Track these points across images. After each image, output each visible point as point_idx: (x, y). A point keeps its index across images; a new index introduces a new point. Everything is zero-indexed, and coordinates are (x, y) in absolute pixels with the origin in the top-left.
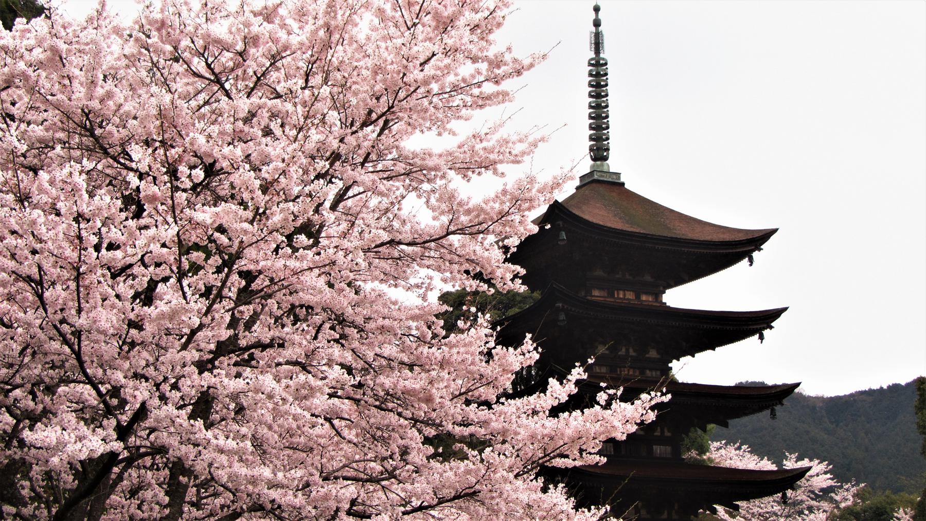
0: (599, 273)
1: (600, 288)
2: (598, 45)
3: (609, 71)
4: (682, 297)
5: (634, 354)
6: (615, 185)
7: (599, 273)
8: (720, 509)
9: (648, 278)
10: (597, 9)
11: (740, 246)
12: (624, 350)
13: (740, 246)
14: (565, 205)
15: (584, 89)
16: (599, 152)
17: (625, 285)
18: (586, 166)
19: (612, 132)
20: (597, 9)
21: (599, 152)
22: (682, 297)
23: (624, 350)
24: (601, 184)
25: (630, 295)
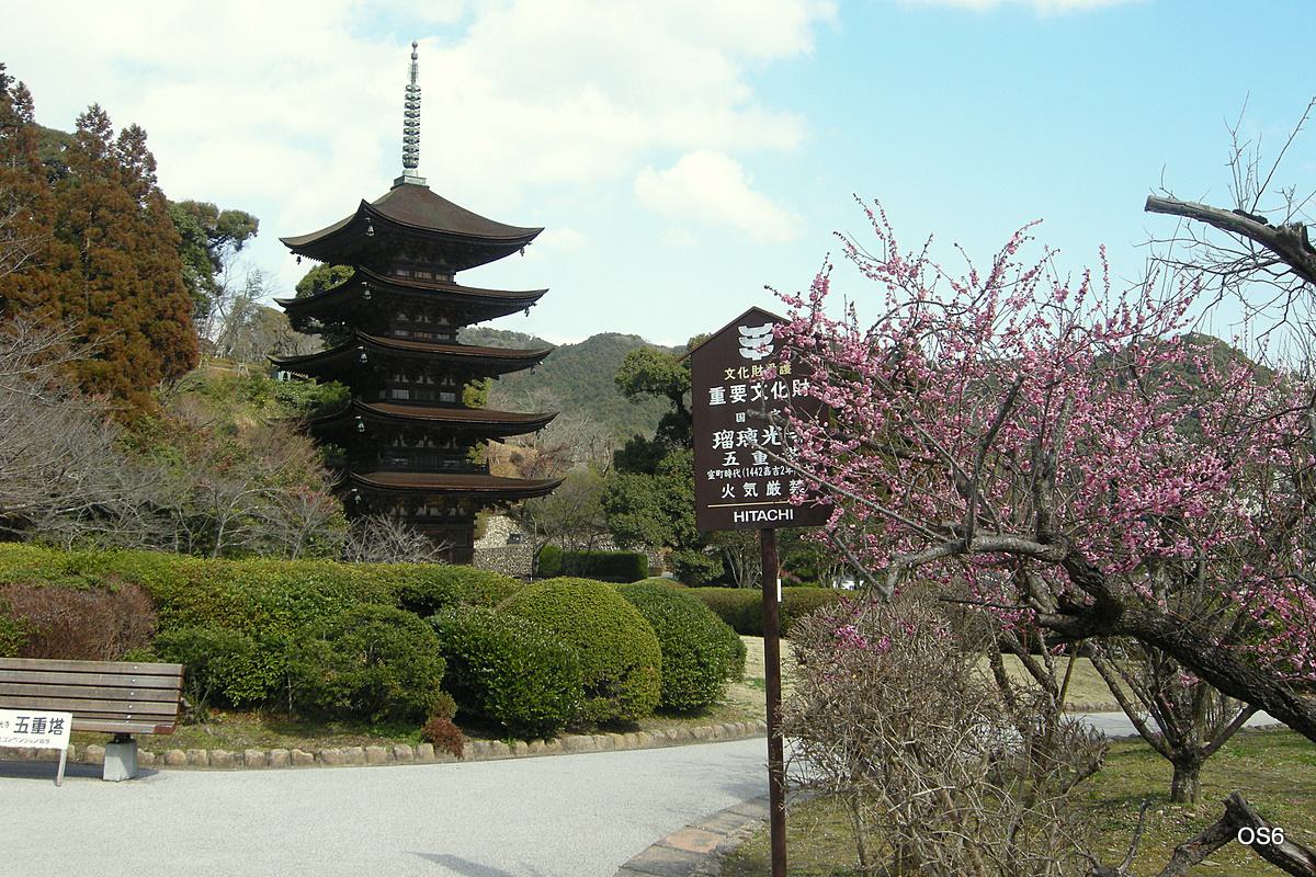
0: (403, 257)
1: (403, 269)
2: (414, 76)
3: (421, 131)
4: (467, 279)
5: (431, 383)
6: (423, 191)
7: (402, 317)
8: (492, 442)
9: (442, 262)
10: (1103, 248)
11: (507, 242)
12: (421, 378)
13: (507, 242)
14: (383, 211)
15: (399, 119)
16: (410, 162)
17: (422, 267)
18: (398, 171)
19: (422, 146)
20: (1103, 248)
21: (410, 162)
22: (467, 279)
23: (421, 378)
24: (407, 191)
25: (428, 276)
